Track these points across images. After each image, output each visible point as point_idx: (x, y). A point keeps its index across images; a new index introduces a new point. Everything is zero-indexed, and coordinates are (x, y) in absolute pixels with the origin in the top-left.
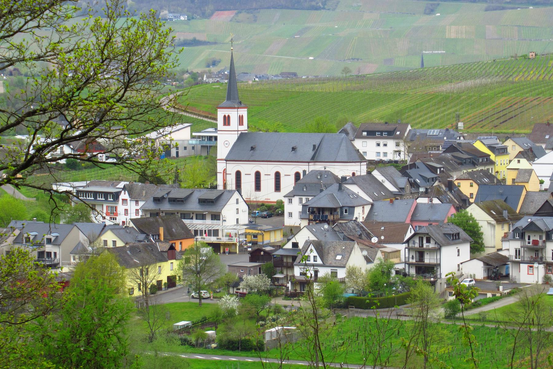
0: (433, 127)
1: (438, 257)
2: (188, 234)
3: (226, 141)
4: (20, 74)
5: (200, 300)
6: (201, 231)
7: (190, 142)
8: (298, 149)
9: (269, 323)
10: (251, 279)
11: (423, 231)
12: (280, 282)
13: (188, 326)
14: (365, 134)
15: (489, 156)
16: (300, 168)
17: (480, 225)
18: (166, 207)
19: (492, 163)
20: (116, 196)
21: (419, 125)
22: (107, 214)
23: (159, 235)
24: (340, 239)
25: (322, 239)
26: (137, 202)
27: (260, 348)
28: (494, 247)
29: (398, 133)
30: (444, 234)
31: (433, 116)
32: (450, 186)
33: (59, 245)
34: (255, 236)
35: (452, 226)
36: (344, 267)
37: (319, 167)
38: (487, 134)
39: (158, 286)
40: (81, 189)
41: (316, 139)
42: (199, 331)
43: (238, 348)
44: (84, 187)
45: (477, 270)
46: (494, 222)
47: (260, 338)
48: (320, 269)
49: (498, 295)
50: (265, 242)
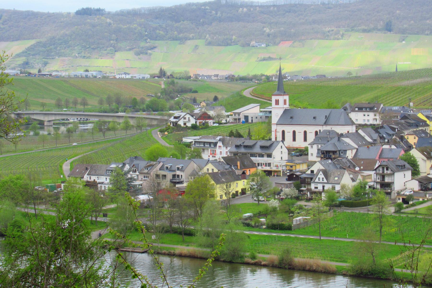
0: (396, 106)
1: (393, 178)
2: (253, 165)
3: (277, 113)
4: (173, 77)
5: (259, 202)
6: (261, 164)
7: (259, 114)
8: (317, 118)
9: (296, 215)
10: (287, 190)
11: (384, 164)
12: (304, 192)
13: (251, 216)
14: (357, 109)
15: (426, 121)
16: (318, 128)
17: (417, 160)
18: (243, 150)
19: (428, 125)
20: (215, 144)
21: (389, 104)
22: (211, 154)
23: (237, 166)
24: (337, 168)
25: (328, 169)
26: (227, 147)
27: (289, 228)
28: (425, 173)
29: (376, 109)
30: (397, 165)
31: (397, 99)
32: (402, 138)
33: (184, 171)
34: (291, 167)
35: (401, 161)
36: (339, 184)
37: (328, 128)
38: (428, 109)
39: (235, 195)
40: (197, 140)
41: (327, 112)
42: (256, 218)
43: (277, 229)
44: (198, 139)
45: (415, 185)
46: (425, 159)
47: (290, 223)
48: (325, 185)
49: (426, 199)
50: (297, 170)
